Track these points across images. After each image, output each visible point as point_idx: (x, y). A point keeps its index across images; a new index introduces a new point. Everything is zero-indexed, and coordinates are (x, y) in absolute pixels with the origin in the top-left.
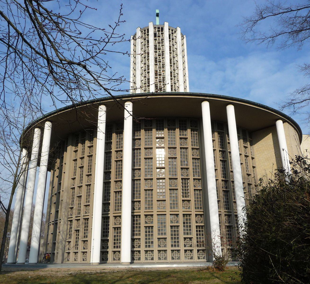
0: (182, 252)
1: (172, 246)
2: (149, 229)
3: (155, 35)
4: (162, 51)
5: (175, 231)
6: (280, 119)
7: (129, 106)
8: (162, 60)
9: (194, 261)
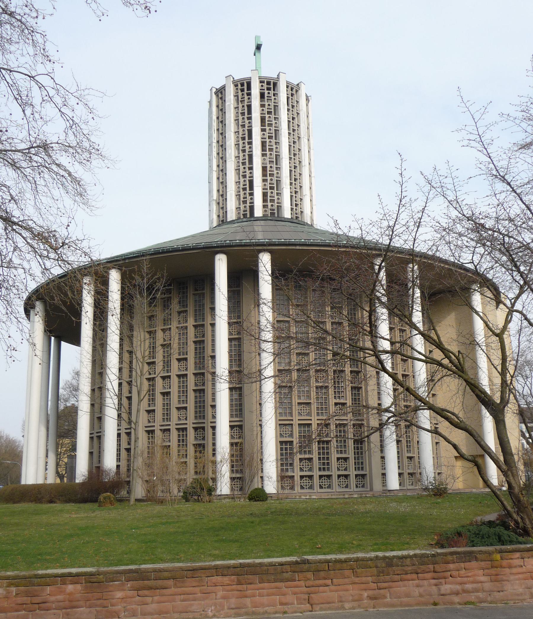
0: (335, 478)
1: (320, 469)
2: (183, 432)
3: (262, 96)
4: (275, 130)
5: (323, 448)
6: (260, 251)
7: (265, 261)
9: (404, 488)
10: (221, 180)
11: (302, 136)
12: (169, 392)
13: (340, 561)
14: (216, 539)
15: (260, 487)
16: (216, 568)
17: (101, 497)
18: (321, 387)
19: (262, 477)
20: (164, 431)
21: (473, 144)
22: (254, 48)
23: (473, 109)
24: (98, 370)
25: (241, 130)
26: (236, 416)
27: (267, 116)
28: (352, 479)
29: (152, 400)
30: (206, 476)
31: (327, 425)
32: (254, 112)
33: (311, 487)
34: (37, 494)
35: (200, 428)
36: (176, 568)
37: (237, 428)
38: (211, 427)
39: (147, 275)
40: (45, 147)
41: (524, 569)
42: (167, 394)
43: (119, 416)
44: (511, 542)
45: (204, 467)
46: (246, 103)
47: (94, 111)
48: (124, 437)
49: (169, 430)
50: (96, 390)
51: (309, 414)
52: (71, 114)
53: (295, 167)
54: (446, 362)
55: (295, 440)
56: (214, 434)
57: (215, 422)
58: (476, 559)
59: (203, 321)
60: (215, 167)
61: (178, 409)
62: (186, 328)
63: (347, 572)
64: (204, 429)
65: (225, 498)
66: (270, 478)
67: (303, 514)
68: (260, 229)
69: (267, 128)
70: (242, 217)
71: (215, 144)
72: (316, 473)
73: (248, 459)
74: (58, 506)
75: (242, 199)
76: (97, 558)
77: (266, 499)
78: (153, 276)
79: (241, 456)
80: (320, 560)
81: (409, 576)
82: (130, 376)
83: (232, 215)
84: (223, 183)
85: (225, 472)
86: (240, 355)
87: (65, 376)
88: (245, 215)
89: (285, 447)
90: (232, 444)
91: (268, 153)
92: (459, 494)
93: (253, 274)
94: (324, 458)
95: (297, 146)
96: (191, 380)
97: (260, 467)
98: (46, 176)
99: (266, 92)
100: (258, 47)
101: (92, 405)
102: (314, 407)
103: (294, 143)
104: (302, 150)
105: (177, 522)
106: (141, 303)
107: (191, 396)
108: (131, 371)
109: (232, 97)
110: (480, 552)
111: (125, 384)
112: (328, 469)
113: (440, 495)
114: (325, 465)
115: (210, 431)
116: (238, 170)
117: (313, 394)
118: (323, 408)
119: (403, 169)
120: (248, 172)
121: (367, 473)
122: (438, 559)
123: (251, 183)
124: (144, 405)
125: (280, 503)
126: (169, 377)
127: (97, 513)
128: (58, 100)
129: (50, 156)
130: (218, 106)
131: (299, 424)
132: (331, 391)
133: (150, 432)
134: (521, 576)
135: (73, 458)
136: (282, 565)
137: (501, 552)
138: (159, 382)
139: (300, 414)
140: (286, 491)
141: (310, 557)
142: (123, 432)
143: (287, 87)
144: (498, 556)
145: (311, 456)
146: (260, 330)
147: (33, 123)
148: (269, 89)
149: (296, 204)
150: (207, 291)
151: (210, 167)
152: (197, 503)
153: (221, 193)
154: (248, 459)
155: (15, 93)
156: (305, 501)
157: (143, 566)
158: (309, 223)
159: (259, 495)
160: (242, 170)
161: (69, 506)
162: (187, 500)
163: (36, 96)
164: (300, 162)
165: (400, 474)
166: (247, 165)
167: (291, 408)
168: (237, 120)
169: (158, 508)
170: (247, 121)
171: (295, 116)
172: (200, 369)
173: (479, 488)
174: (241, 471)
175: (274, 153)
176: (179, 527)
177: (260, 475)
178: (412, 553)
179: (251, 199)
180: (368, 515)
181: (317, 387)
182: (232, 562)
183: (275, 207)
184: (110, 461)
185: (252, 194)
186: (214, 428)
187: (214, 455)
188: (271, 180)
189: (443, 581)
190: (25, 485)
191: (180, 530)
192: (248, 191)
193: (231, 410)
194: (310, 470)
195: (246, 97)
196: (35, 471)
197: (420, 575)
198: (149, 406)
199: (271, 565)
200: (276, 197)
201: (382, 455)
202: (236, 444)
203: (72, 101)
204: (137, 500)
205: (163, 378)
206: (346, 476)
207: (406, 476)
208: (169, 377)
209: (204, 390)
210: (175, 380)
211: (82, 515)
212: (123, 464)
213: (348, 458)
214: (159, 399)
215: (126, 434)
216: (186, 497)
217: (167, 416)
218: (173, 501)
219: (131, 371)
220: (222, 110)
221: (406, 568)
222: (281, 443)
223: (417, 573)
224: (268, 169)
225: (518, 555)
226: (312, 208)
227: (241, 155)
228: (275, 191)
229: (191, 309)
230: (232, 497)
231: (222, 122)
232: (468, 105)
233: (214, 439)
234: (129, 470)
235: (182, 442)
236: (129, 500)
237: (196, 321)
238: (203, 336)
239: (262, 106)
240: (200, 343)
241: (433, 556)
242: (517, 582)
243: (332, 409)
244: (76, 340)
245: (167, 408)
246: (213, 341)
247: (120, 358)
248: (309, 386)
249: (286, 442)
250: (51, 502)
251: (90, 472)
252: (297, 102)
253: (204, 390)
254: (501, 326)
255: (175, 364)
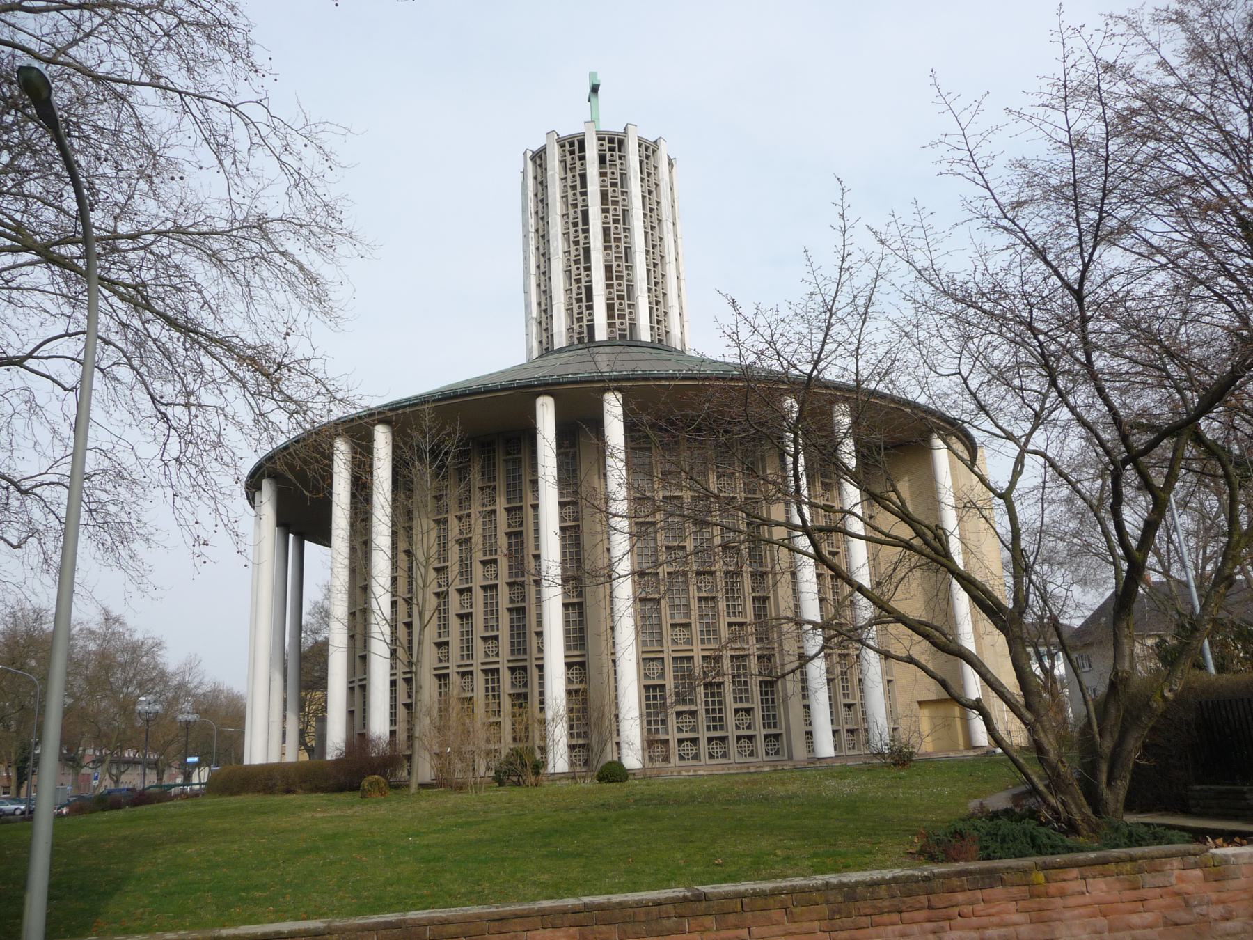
0: (732, 741)
1: (708, 728)
3: (602, 160)
6: (607, 390)
7: (613, 410)
8: (620, 198)
10: (543, 288)
11: (664, 218)
12: (471, 614)
13: (764, 895)
14: (544, 851)
15: (616, 759)
16: (542, 913)
17: (365, 783)
18: (706, 599)
19: (618, 744)
20: (463, 674)
21: (957, 168)
22: (588, 90)
23: (957, 107)
24: (360, 583)
25: (571, 211)
26: (576, 648)
27: (610, 189)
28: (760, 740)
29: (444, 626)
30: (530, 744)
31: (717, 659)
32: (591, 186)
33: (696, 757)
34: (269, 780)
35: (519, 668)
36: (470, 916)
37: (577, 667)
38: (537, 666)
39: (430, 429)
40: (261, 224)
41: (1087, 899)
42: (468, 616)
43: (393, 653)
44: (1055, 850)
45: (527, 729)
46: (578, 172)
47: (333, 157)
48: (401, 686)
49: (471, 673)
50: (358, 613)
51: (689, 641)
52: (296, 165)
53: (655, 265)
54: (917, 542)
55: (670, 683)
56: (541, 677)
57: (542, 659)
58: (1003, 883)
59: (521, 501)
60: (533, 270)
61: (485, 639)
62: (494, 512)
63: (776, 915)
64: (526, 669)
65: (560, 779)
66: (630, 744)
67: (686, 803)
68: (604, 357)
69: (611, 208)
70: (576, 342)
71: (532, 235)
72: (703, 735)
73: (595, 715)
74: (296, 799)
75: (575, 315)
76: (341, 894)
77: (627, 779)
78: (439, 432)
79: (585, 710)
80: (728, 893)
81: (886, 918)
82: (410, 591)
83: (561, 340)
84: (546, 293)
85: (559, 736)
86: (578, 553)
87: (312, 594)
88: (580, 340)
89: (652, 693)
90: (569, 693)
91: (613, 244)
92: (929, 761)
93: (597, 424)
94: (714, 710)
95: (657, 233)
96: (504, 593)
97: (614, 728)
98: (265, 273)
99: (608, 154)
100: (595, 89)
101: (352, 637)
102: (696, 628)
103: (653, 228)
104: (665, 239)
105: (483, 821)
106: (423, 474)
107: (505, 618)
108: (410, 583)
109: (557, 163)
110: (1009, 870)
111: (401, 603)
112: (722, 728)
113: (904, 764)
114: (717, 721)
115: (536, 672)
116: (568, 272)
117: (695, 613)
118: (709, 632)
119: (845, 206)
120: (584, 274)
121: (783, 731)
122: (936, 884)
123: (589, 290)
124: (431, 634)
125: (648, 785)
126: (470, 590)
127: (358, 809)
128: (274, 141)
129: (270, 241)
130: (535, 178)
131: (674, 658)
132: (722, 605)
133: (442, 678)
134: (1082, 911)
135: (322, 720)
136: (660, 904)
137: (1045, 867)
138: (454, 598)
139: (674, 642)
140: (657, 765)
141: (708, 889)
142: (400, 678)
143: (640, 145)
144: (1040, 877)
145: (693, 708)
146: (607, 499)
147: (237, 180)
148: (612, 149)
149: (658, 319)
150: (525, 455)
151: (527, 268)
152: (517, 789)
153: (543, 307)
154: (595, 715)
155: (207, 134)
156: (688, 781)
157: (412, 915)
158: (679, 348)
159: (614, 773)
160: (574, 272)
161: (315, 798)
162: (501, 783)
163: (240, 136)
164: (662, 257)
165: (835, 732)
166: (582, 265)
167: (661, 633)
168: (565, 197)
169: (454, 799)
170: (580, 199)
171: (653, 189)
172: (517, 576)
173: (957, 750)
174: (586, 735)
175: (622, 245)
176: (485, 831)
177: (615, 739)
178: (888, 874)
179: (590, 314)
180: (793, 801)
181: (700, 599)
182: (570, 902)
183: (627, 326)
184: (379, 725)
185: (590, 307)
186: (541, 668)
187: (542, 709)
188: (619, 285)
189: (946, 924)
190: (250, 766)
191: (487, 836)
192: (584, 303)
193: (567, 639)
194: (694, 729)
195: (578, 163)
196: (264, 744)
197: (904, 915)
198: (440, 636)
199: (640, 905)
200: (627, 311)
201: (806, 702)
202: (577, 691)
203: (298, 143)
204: (422, 786)
205: (461, 592)
206: (750, 738)
207: (843, 734)
208: (470, 590)
209: (524, 608)
210: (478, 595)
211: (333, 813)
212: (401, 728)
213: (752, 709)
214: (455, 624)
215: (405, 682)
216: (499, 780)
217: (467, 651)
218: (478, 786)
219: (410, 583)
220: (541, 183)
221: (879, 904)
222: (647, 688)
223: (900, 912)
224: (614, 268)
225: (1075, 872)
226: (682, 326)
227: (573, 248)
228: (626, 302)
229: (501, 484)
230: (571, 776)
231: (542, 201)
232: (949, 99)
233: (542, 685)
234: (410, 738)
235: (492, 690)
236: (408, 786)
237: (509, 502)
238: (521, 525)
239: (603, 174)
240: (516, 536)
241: (927, 879)
242: (1078, 922)
243: (725, 633)
244: (324, 537)
245: (467, 638)
246: (537, 531)
247: (393, 564)
248: (688, 599)
249: (654, 687)
250: (288, 791)
251: (349, 743)
252: (656, 168)
253: (524, 608)
254: (1006, 485)
255: (478, 570)
